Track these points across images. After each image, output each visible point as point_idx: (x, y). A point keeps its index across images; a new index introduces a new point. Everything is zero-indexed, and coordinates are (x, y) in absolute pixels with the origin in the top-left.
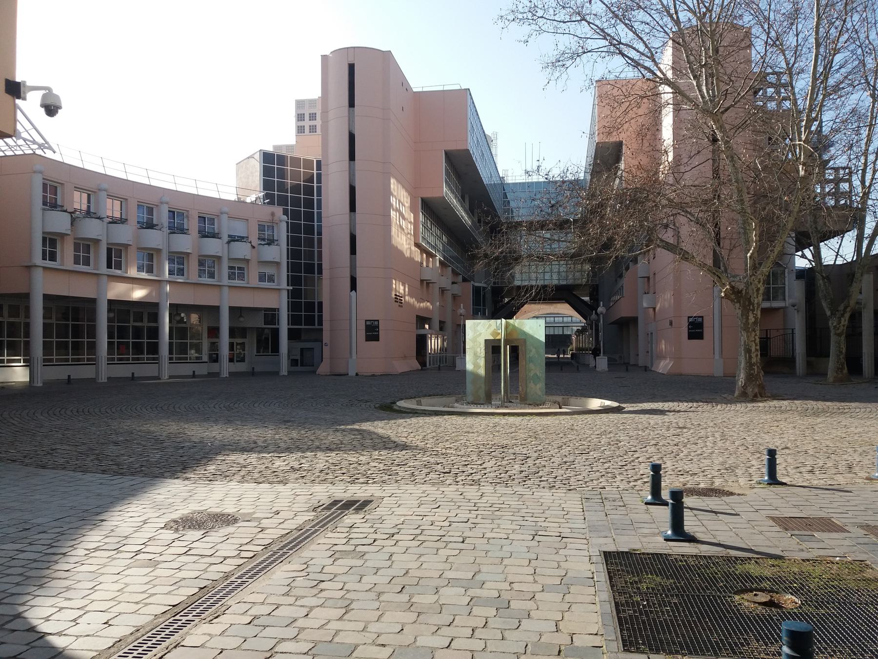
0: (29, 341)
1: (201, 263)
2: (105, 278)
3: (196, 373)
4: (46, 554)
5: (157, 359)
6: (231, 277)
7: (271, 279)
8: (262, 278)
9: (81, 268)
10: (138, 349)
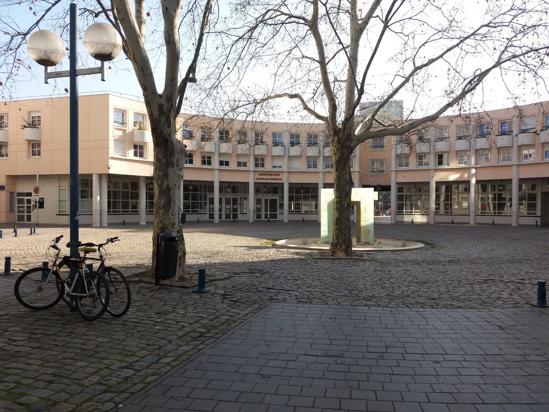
0: (519, 201)
1: (256, 159)
2: (432, 171)
3: (495, 223)
4: (18, 375)
5: (137, 211)
6: (256, 165)
7: (245, 165)
8: (239, 164)
9: (206, 166)
10: (125, 205)
